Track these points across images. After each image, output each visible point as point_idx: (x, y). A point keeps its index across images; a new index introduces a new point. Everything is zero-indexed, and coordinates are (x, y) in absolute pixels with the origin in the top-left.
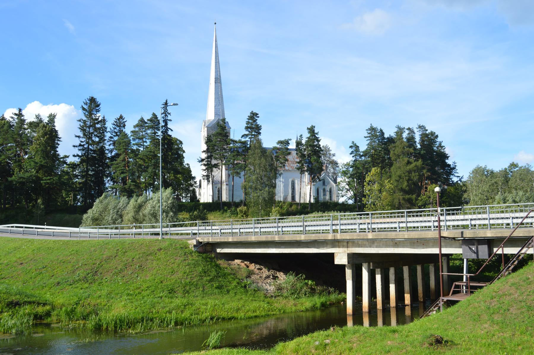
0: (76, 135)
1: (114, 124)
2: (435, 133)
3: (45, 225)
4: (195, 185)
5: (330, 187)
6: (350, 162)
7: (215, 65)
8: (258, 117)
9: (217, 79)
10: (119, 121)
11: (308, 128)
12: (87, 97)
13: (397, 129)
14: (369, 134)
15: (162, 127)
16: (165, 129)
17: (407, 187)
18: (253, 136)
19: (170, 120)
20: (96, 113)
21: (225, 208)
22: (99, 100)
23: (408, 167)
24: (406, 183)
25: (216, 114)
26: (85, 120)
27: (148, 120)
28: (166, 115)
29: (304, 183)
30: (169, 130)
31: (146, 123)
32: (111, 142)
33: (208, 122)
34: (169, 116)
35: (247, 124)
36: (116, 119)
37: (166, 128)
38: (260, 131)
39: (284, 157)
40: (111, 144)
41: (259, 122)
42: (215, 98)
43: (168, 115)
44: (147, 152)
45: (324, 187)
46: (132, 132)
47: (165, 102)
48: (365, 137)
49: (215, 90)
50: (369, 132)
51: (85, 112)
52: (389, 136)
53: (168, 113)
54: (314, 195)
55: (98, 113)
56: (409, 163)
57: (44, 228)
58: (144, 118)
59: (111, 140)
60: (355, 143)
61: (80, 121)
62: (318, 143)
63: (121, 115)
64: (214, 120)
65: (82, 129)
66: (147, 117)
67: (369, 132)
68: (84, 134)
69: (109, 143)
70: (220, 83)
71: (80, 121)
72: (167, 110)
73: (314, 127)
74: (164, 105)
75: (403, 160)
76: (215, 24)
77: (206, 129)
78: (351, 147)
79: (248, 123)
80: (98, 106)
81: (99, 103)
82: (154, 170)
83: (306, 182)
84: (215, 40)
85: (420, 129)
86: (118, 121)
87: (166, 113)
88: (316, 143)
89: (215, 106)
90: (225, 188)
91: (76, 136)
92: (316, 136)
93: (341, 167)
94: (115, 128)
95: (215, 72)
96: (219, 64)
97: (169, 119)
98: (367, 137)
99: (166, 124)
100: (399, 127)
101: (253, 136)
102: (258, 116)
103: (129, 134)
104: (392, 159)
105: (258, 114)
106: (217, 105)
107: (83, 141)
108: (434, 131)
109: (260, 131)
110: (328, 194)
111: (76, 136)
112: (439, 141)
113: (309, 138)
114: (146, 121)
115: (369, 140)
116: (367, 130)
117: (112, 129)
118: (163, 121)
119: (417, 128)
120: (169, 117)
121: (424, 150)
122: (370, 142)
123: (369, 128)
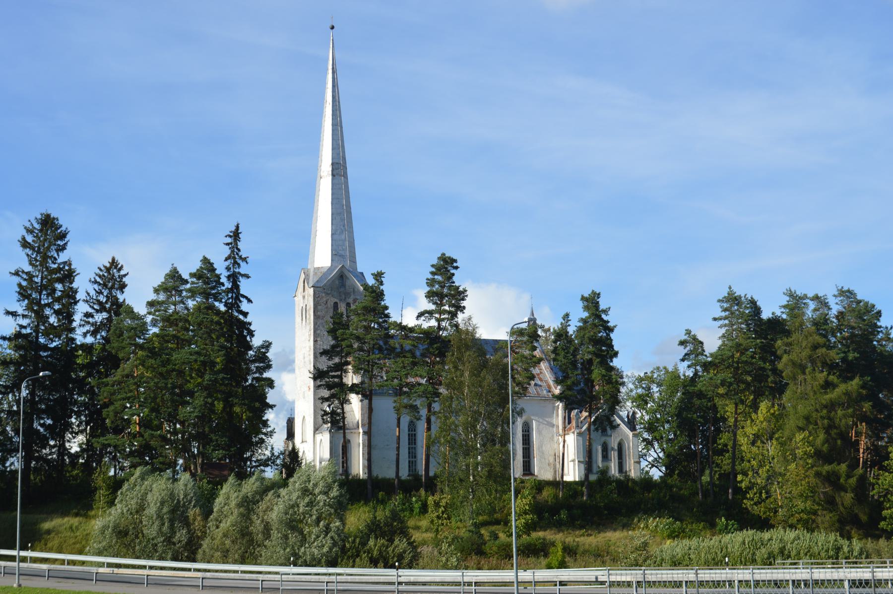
0: (8, 310)
1: (95, 282)
2: (873, 306)
3: (28, 550)
4: (264, 431)
5: (618, 440)
6: (652, 372)
7: (333, 130)
8: (457, 268)
9: (336, 166)
10: (109, 273)
11: (582, 296)
12: (33, 215)
13: (788, 298)
14: (725, 310)
15: (228, 291)
16: (232, 296)
17: (826, 445)
18: (446, 316)
19: (247, 276)
20: (56, 255)
21: (381, 495)
22: (65, 222)
23: (828, 397)
24: (822, 436)
25: (336, 254)
26: (28, 273)
27: (192, 275)
28: (235, 263)
29: (555, 429)
30: (242, 299)
31: (186, 282)
32: (87, 328)
33: (315, 274)
34: (243, 264)
35: (428, 284)
36: (101, 270)
37: (235, 294)
38: (463, 303)
39: (527, 370)
40: (88, 332)
41: (460, 280)
42: (332, 214)
43: (239, 261)
44: (191, 355)
45: (603, 439)
46: (151, 304)
47: (233, 229)
48: (715, 319)
49: (332, 194)
50: (725, 305)
51: (28, 251)
52: (771, 316)
53: (241, 257)
54: (582, 460)
55: (60, 254)
56: (828, 385)
57: (190, 570)
58: (179, 269)
59: (88, 323)
60: (692, 333)
61: (16, 273)
62: (608, 335)
63: (113, 259)
64: (330, 269)
65: (23, 293)
66: (188, 268)
67: (725, 305)
68: (29, 308)
69: (84, 330)
70: (345, 176)
71: (16, 273)
72: (239, 250)
73: (599, 294)
74: (230, 236)
75: (814, 379)
76: (333, 28)
77: (311, 291)
78: (682, 343)
79: (431, 283)
80: (63, 236)
81: (63, 229)
82: (209, 400)
83: (558, 427)
84: (333, 68)
85: (842, 298)
86: (106, 274)
87: (235, 257)
88: (602, 334)
89: (332, 235)
90: (361, 442)
91: (8, 313)
92: (604, 316)
93: (631, 386)
94: (100, 293)
95: (333, 149)
96: (341, 127)
97: (242, 273)
98: (720, 319)
99: (236, 287)
100: (791, 295)
101: (446, 316)
102: (455, 264)
103: (141, 309)
104: (784, 374)
105: (455, 261)
106: (336, 230)
107: (25, 324)
108: (878, 307)
109: (463, 303)
110: (614, 455)
111: (8, 313)
112: (884, 325)
113: (584, 321)
114: (185, 276)
115: (725, 325)
116: (719, 301)
117: (93, 293)
118: (229, 277)
119: (835, 296)
120: (244, 269)
121: (854, 350)
122: (727, 330)
123: (725, 297)
